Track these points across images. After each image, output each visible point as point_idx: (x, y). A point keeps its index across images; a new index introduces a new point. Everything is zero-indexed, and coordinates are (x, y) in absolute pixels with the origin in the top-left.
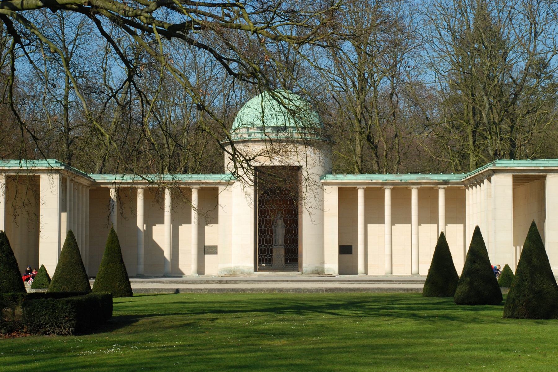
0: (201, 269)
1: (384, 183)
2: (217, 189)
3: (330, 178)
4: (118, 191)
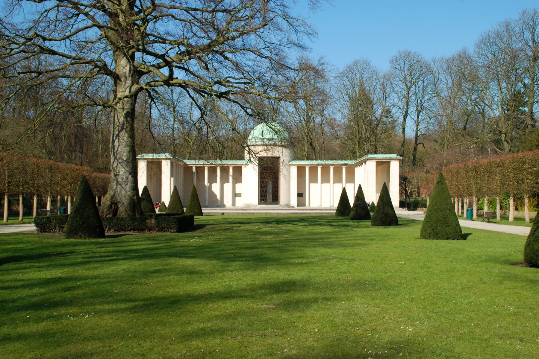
0: (234, 204)
1: (318, 165)
2: (241, 167)
3: (294, 162)
4: (196, 168)
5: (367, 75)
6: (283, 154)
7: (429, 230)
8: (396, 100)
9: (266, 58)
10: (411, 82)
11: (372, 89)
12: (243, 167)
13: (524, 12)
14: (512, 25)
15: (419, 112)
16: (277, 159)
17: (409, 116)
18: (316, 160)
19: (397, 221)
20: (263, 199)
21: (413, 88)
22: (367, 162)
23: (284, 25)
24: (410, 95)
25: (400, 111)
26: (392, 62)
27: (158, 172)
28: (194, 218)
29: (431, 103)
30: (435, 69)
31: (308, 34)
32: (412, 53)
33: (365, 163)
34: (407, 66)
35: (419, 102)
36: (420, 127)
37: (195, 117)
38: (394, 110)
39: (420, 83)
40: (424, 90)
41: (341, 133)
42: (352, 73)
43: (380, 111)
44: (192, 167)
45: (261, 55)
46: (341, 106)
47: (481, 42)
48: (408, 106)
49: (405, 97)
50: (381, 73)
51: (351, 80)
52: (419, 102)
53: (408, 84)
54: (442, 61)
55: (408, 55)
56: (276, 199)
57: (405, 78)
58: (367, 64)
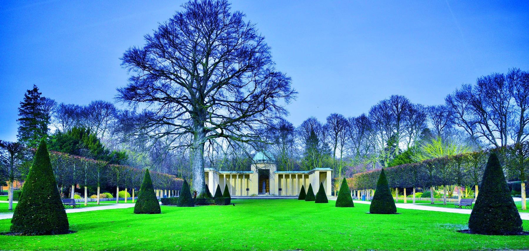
5: (315, 126)
6: (272, 169)
7: (339, 203)
8: (330, 139)
9: (265, 124)
10: (338, 130)
11: (318, 133)
12: (250, 174)
13: (392, 96)
14: (387, 102)
15: (342, 146)
16: (268, 171)
17: (337, 148)
18: (289, 171)
19: (396, 211)
20: (260, 191)
21: (339, 133)
22: (315, 172)
23: (274, 109)
24: (337, 137)
25: (333, 145)
26: (328, 119)
27: (387, 212)
28: (65, 214)
29: (349, 141)
30: (350, 123)
31: (285, 113)
32: (338, 115)
33: (314, 173)
34: (335, 122)
35: (342, 140)
36: (343, 153)
37: (225, 149)
38: (330, 144)
39: (343, 131)
40: (345, 134)
41: (302, 156)
42: (307, 125)
43: (322, 145)
44: (223, 175)
45: (262, 123)
46: (302, 142)
47: (372, 111)
48: (336, 143)
49: (334, 138)
50: (322, 125)
51: (307, 129)
52: (342, 140)
53: (336, 131)
54: (354, 119)
55: (336, 116)
56: (268, 190)
57: (335, 127)
58: (315, 120)
